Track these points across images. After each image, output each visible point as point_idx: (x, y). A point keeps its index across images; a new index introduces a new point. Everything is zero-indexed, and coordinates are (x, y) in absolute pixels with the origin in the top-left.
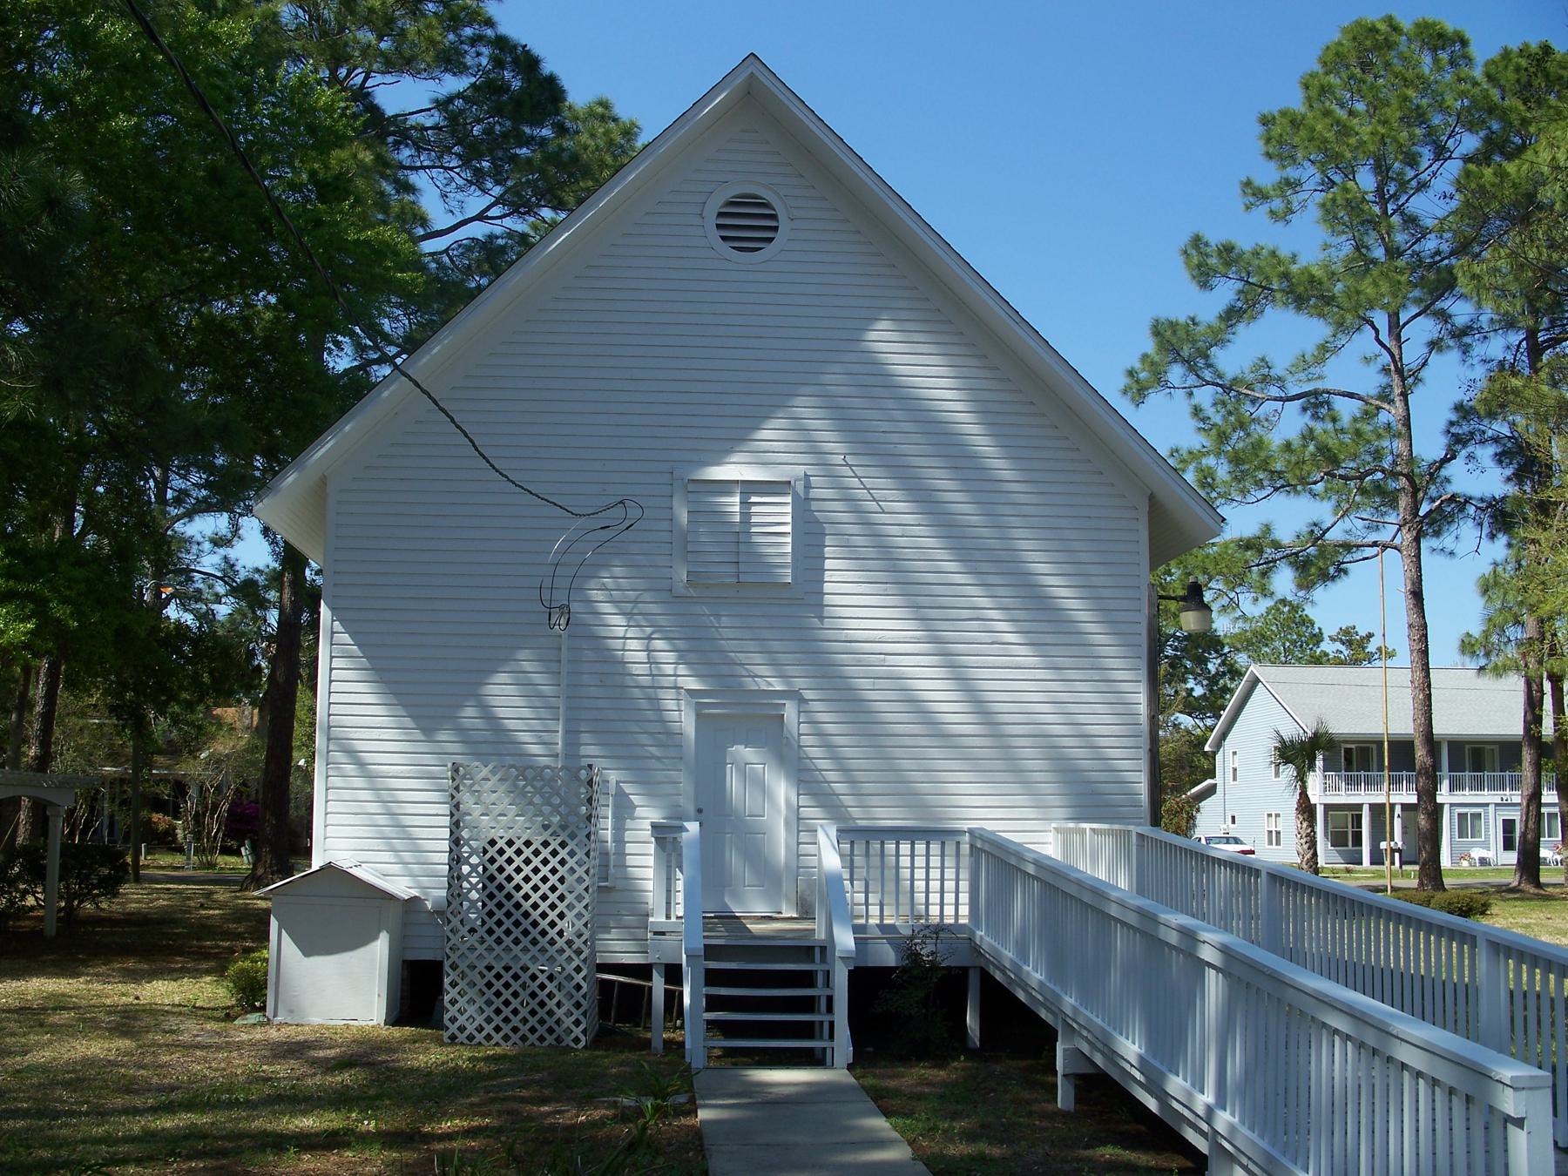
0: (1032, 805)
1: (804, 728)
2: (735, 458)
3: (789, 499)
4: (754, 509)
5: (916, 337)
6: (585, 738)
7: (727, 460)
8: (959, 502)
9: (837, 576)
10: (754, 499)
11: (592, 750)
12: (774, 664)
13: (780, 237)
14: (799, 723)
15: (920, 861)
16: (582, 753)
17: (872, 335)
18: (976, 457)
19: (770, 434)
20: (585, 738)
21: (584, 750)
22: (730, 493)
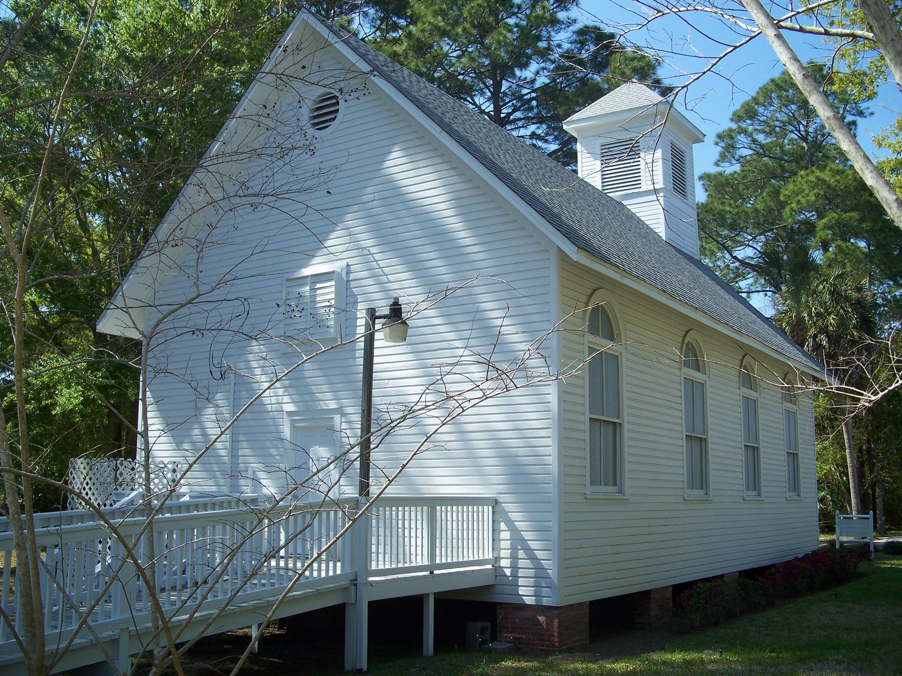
0: (477, 474)
1: (344, 426)
2: (315, 260)
3: (333, 283)
4: (318, 292)
5: (418, 157)
6: (241, 438)
7: (310, 264)
8: (441, 270)
9: (543, 433)
10: (318, 286)
11: (247, 452)
12: (333, 391)
13: (339, 115)
14: (341, 422)
15: (407, 514)
16: (240, 454)
17: (388, 164)
18: (445, 233)
19: (335, 241)
20: (244, 444)
21: (241, 452)
22: (305, 285)
